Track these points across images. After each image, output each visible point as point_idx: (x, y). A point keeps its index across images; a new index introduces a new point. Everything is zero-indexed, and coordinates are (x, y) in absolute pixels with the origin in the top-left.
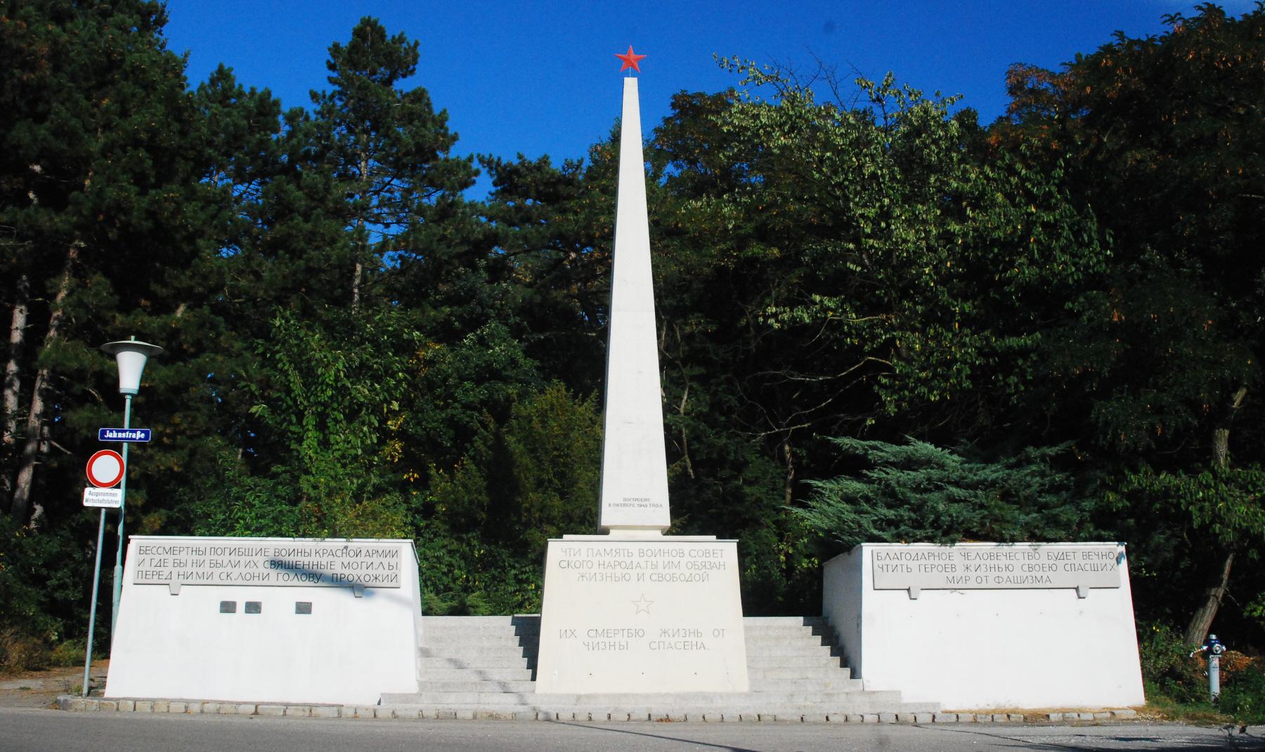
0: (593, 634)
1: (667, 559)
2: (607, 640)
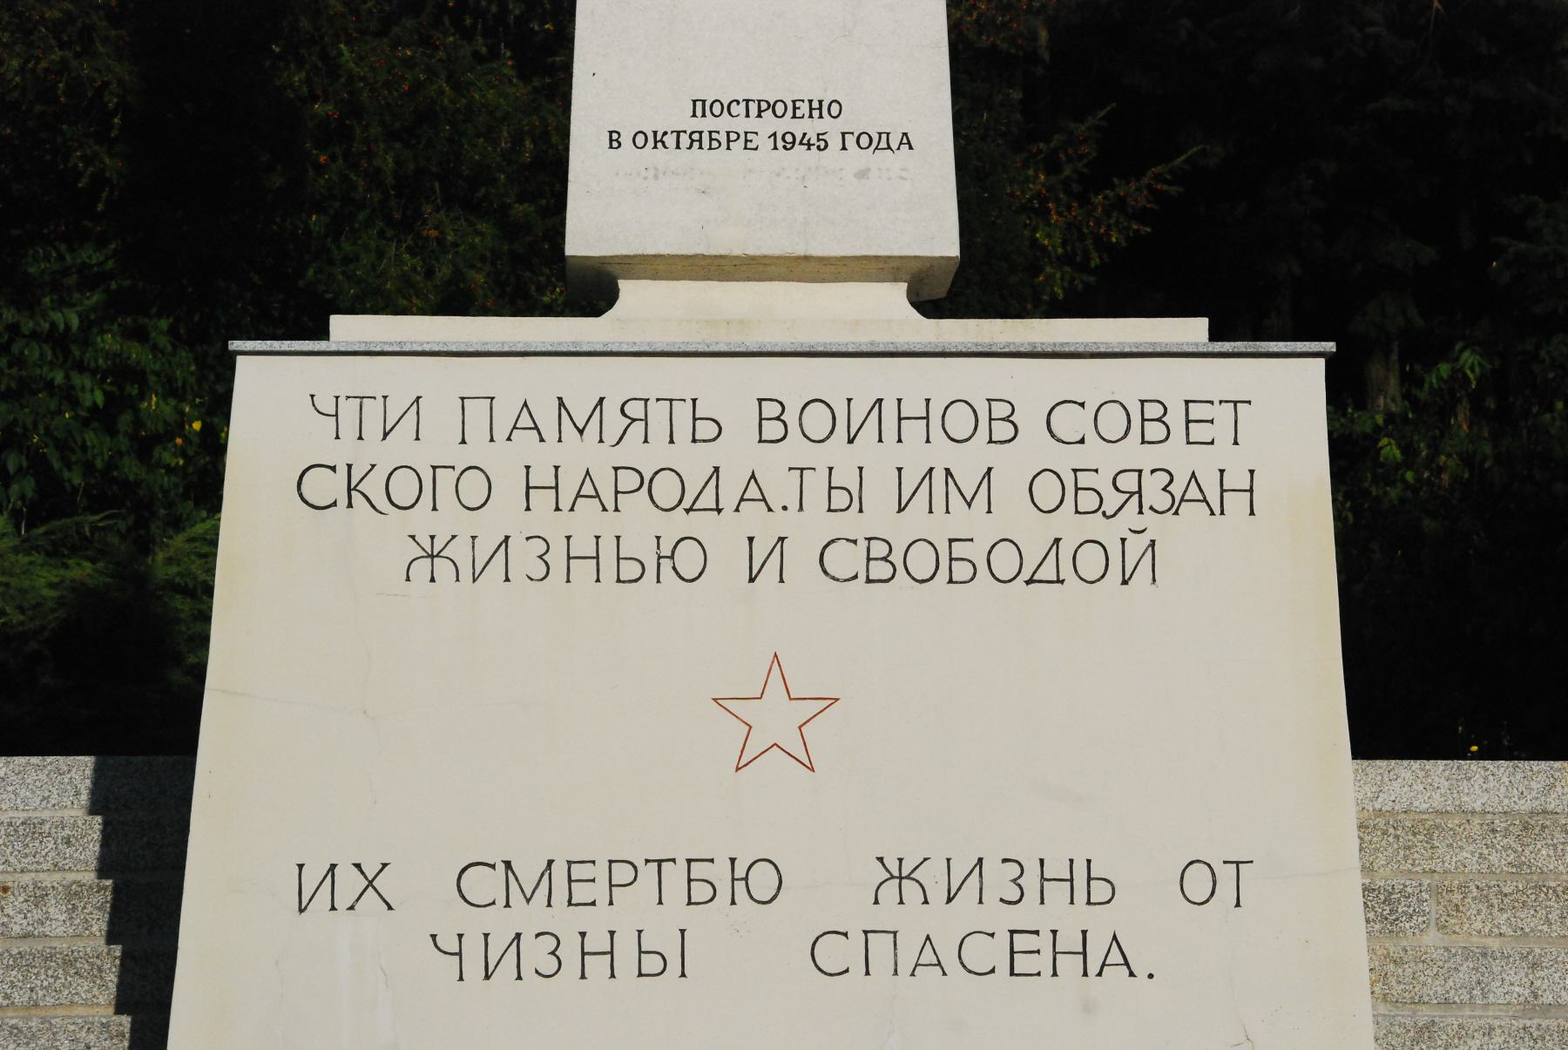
0: (483, 885)
1: (916, 455)
2: (567, 923)
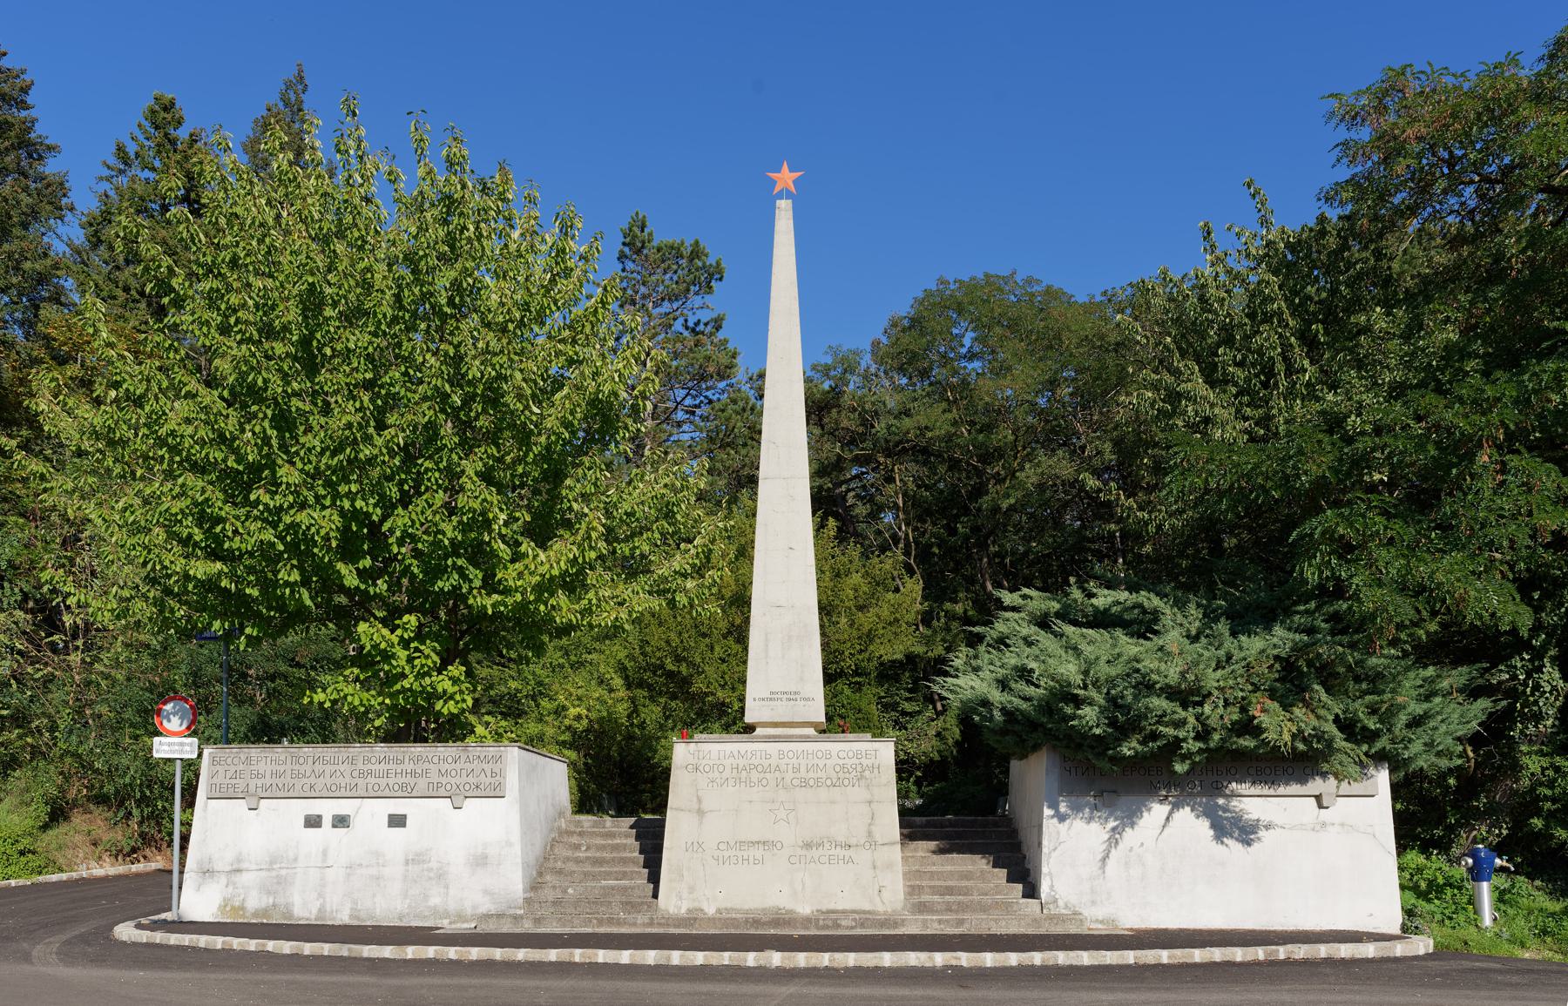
2: (740, 854)
